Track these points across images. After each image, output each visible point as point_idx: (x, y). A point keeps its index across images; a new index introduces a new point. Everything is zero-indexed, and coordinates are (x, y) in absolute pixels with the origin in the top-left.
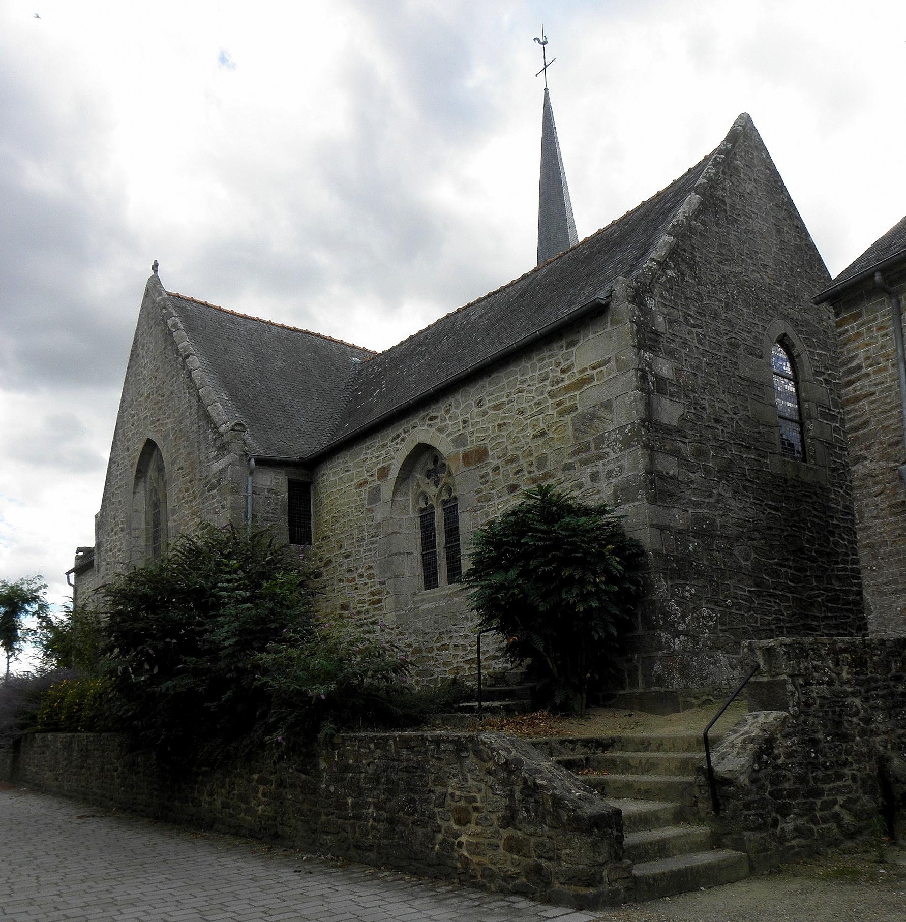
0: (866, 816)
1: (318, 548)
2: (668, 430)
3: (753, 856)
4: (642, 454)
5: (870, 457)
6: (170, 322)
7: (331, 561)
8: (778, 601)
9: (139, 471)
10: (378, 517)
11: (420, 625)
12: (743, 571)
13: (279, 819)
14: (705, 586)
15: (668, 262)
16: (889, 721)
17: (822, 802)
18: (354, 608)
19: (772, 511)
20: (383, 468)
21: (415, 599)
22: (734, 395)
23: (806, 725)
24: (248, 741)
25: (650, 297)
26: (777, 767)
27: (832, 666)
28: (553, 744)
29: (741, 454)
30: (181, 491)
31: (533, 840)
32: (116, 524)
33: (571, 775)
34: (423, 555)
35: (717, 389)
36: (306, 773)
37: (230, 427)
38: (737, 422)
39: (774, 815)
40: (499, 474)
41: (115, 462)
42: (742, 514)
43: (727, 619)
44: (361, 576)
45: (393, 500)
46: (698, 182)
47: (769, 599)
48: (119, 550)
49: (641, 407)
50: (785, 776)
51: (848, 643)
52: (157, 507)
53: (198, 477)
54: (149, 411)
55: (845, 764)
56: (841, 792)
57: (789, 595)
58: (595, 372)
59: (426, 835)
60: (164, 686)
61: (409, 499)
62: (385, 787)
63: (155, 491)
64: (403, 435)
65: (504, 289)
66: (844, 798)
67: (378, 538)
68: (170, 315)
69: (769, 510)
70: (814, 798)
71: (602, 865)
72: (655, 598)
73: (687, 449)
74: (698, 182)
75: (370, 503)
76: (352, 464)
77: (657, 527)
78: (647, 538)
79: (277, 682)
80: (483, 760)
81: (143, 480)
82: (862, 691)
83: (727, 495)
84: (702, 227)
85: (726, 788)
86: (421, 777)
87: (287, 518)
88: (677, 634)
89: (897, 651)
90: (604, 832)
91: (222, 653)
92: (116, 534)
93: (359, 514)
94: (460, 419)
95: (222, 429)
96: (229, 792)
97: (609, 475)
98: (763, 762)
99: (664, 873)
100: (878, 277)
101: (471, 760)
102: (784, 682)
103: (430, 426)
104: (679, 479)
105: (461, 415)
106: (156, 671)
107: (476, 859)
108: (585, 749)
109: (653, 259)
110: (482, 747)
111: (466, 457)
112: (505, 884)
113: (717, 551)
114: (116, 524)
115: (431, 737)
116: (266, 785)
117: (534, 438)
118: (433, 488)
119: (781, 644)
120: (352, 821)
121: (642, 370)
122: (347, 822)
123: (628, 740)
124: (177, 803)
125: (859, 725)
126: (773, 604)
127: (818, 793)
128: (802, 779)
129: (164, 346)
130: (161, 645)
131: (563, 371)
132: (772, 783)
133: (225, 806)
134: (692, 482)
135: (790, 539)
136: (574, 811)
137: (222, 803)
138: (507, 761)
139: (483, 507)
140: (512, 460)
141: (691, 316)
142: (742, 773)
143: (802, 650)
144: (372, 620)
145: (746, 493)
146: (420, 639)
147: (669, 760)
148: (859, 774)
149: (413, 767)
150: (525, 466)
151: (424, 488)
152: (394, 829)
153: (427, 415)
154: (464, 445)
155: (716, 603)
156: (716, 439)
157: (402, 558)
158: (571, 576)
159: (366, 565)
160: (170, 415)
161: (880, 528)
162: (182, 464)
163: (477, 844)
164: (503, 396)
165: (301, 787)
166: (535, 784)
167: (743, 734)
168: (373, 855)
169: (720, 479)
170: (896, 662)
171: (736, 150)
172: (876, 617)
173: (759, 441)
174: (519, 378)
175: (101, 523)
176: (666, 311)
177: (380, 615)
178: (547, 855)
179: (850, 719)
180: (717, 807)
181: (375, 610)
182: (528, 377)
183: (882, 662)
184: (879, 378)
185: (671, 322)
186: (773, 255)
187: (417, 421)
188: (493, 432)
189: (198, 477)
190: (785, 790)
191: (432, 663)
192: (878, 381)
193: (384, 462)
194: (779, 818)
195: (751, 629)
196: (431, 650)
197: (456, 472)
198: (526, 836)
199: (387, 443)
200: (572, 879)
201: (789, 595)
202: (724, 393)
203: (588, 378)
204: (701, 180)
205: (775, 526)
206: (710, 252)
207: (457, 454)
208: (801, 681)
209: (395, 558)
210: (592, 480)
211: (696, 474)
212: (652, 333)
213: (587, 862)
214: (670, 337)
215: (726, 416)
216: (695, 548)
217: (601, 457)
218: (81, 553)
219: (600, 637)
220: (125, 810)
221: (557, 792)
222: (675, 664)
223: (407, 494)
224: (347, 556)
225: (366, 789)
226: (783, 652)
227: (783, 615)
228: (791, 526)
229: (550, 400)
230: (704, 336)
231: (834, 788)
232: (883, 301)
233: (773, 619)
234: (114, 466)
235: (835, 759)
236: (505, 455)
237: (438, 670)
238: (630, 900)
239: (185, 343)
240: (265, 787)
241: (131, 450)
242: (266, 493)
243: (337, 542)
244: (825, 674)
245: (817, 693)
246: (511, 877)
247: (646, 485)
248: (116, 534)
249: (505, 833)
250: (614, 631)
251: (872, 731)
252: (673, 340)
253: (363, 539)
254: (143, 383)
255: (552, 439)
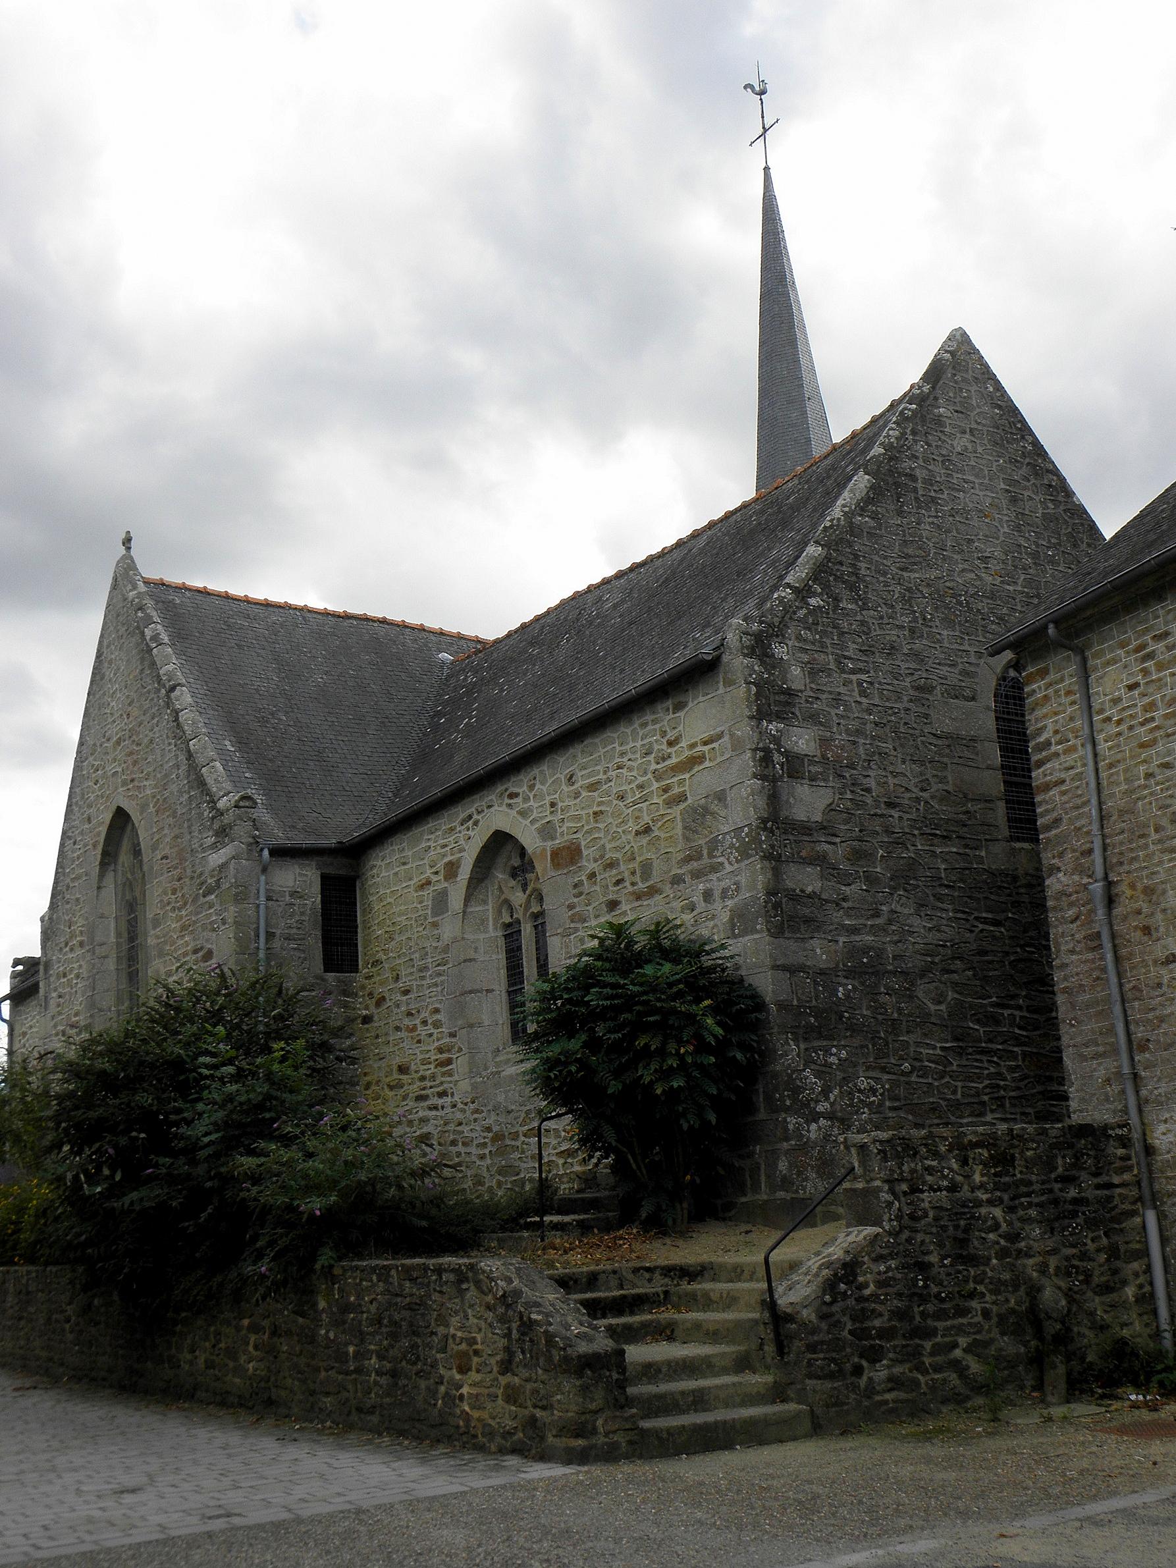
0: (1005, 1364)
1: (367, 978)
2: (806, 829)
3: (818, 1411)
4: (762, 868)
5: (1063, 868)
6: (148, 633)
7: (384, 998)
8: (995, 1059)
9: (105, 853)
10: (445, 936)
11: (501, 1098)
12: (933, 1020)
13: (273, 1379)
14: (862, 1047)
15: (811, 587)
16: (1049, 1238)
17: (933, 1346)
18: (416, 1072)
19: (986, 927)
20: (450, 864)
21: (498, 1059)
22: (922, 763)
23: (910, 1244)
24: (236, 1274)
25: (780, 643)
26: (860, 1299)
27: (955, 1166)
28: (624, 1273)
29: (932, 848)
30: (165, 893)
31: (529, 1386)
32: (73, 936)
33: (579, 1309)
34: (509, 993)
35: (892, 758)
36: (303, 1314)
37: (233, 802)
38: (927, 802)
39: (856, 1360)
40: (595, 883)
41: (70, 838)
42: (933, 937)
43: (901, 1091)
44: (425, 1023)
45: (464, 912)
46: (872, 453)
47: (978, 1057)
48: (77, 976)
49: (761, 802)
50: (873, 1311)
51: (982, 1134)
52: (132, 908)
53: (189, 871)
54: (120, 765)
55: (972, 1295)
56: (965, 1332)
57: (1015, 1049)
58: (706, 748)
59: (428, 1388)
60: (127, 1200)
61: (487, 909)
62: (388, 1329)
63: (129, 885)
64: (475, 817)
65: (652, 561)
66: (970, 1340)
67: (445, 968)
68: (149, 621)
69: (981, 926)
70: (920, 1339)
71: (596, 1412)
72: (778, 1068)
73: (837, 852)
74: (872, 453)
75: (435, 914)
76: (410, 853)
77: (784, 968)
78: (767, 984)
79: (268, 1195)
80: (483, 1292)
81: (112, 867)
82: (1006, 1197)
83: (906, 911)
84: (872, 524)
85: (788, 1325)
86: (423, 1315)
87: (319, 933)
88: (814, 1117)
89: (1067, 1143)
90: (600, 1375)
91: (203, 1154)
92: (72, 950)
93: (421, 929)
94: (547, 801)
95: (222, 804)
96: (214, 1346)
97: (724, 894)
98: (839, 1293)
99: (683, 1426)
100: (1051, 630)
101: (472, 1293)
102: (879, 1190)
103: (509, 805)
104: (823, 897)
105: (549, 794)
106: (118, 1177)
107: (475, 1414)
108: (666, 1280)
109: (788, 585)
110: (481, 1277)
111: (555, 854)
112: (503, 1442)
113: (886, 994)
114: (73, 936)
115: (433, 1265)
116: (257, 1333)
117: (636, 835)
118: (520, 894)
119: (875, 1141)
120: (354, 1376)
121: (764, 750)
122: (349, 1377)
123: (722, 1266)
124: (149, 1365)
125: (998, 1243)
126: (986, 1065)
127: (930, 1333)
128: (902, 1315)
129: (140, 667)
130: (123, 1141)
131: (670, 744)
132: (854, 1319)
133: (210, 1365)
134: (844, 900)
135: (1021, 966)
136: (565, 1349)
137: (206, 1361)
138: (505, 1292)
139: (576, 930)
140: (611, 865)
141: (850, 658)
142: (806, 1307)
143: (907, 1147)
144: (440, 1089)
145: (941, 905)
146: (502, 1119)
147: (609, 1289)
148: (995, 1308)
149: (416, 1304)
150: (626, 874)
151: (508, 894)
152: (397, 1384)
153: (506, 790)
154: (553, 838)
155: (883, 1070)
156: (888, 831)
157: (479, 997)
158: (647, 1046)
159: (430, 1007)
160: (148, 774)
161: (1076, 967)
162: (167, 851)
163: (477, 1395)
164: (598, 774)
165: (298, 1335)
166: (530, 1318)
167: (824, 1257)
168: (375, 1419)
169: (894, 889)
170: (1064, 1157)
171: (938, 392)
172: (1077, 1091)
173: (965, 826)
174: (618, 749)
175: (50, 929)
176: (806, 658)
177: (450, 1082)
178: (540, 1404)
179: (983, 1235)
180: (781, 1350)
181: (443, 1074)
182: (628, 747)
183: (1040, 1157)
184: (1069, 760)
185: (814, 672)
186: (1002, 538)
187: (493, 797)
188: (588, 823)
189: (189, 871)
190: (874, 1328)
191: (517, 1155)
192: (1067, 764)
193: (452, 855)
194: (865, 1363)
195: (943, 1103)
196: (515, 1136)
197: (543, 875)
198: (523, 1383)
199: (455, 826)
200: (564, 1430)
201: (1015, 1049)
202: (904, 762)
203: (699, 757)
204: (877, 450)
205: (994, 948)
206: (886, 558)
207: (544, 849)
208: (904, 1187)
209: (468, 998)
210: (705, 901)
211: (853, 886)
212: (783, 693)
213: (576, 1409)
214: (812, 694)
215: (908, 795)
216: (847, 996)
217: (715, 868)
218: (20, 968)
219: (691, 1127)
220: (80, 1380)
221: (551, 1329)
222: (811, 1158)
223: (485, 902)
224: (406, 992)
225: (368, 1334)
226: (876, 1151)
227: (1005, 1079)
228: (1022, 947)
229: (655, 783)
230: (871, 683)
231: (953, 1327)
232: (1069, 657)
233: (986, 1087)
234: (69, 842)
235: (957, 1289)
236: (602, 857)
237: (525, 1165)
238: (634, 1456)
239: (170, 667)
240: (257, 1336)
241: (94, 822)
242: (288, 898)
243: (393, 970)
244: (944, 1177)
245: (930, 1202)
246: (509, 1433)
247: (768, 911)
248: (72, 950)
249: (503, 1380)
250: (712, 1118)
251: (1019, 1251)
252: (818, 698)
253: (426, 968)
254: (110, 720)
255: (658, 838)
